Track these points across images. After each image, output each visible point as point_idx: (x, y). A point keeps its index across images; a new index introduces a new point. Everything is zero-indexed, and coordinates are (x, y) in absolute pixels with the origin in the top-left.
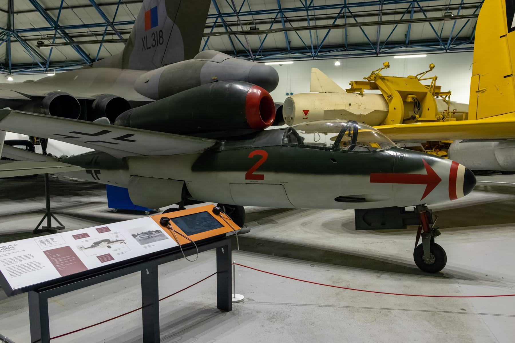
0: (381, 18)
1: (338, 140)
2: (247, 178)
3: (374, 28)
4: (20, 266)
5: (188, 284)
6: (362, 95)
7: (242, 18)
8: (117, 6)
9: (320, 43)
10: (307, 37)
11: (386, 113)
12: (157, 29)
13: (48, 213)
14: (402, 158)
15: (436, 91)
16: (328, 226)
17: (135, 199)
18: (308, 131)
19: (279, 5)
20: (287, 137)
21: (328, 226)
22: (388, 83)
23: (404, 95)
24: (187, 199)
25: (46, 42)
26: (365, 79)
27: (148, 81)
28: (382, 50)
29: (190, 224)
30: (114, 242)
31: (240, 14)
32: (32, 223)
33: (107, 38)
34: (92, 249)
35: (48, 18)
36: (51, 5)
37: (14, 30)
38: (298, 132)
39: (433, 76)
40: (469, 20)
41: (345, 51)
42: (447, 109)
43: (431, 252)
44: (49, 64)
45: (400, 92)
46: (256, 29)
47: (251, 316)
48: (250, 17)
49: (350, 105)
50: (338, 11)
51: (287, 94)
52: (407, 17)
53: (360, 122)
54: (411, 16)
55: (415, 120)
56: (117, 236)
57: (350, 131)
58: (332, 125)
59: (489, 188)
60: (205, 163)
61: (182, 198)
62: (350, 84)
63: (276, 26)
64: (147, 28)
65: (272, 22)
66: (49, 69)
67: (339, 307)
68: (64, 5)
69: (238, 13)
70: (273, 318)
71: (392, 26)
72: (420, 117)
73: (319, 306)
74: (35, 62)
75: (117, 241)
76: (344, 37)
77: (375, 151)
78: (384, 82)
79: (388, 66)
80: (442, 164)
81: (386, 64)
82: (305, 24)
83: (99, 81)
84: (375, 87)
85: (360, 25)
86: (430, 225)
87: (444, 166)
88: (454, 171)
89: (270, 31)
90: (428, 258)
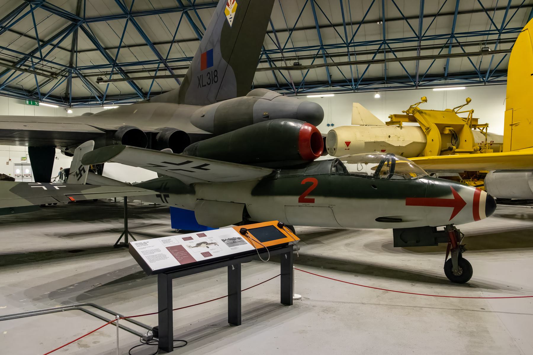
0: (420, 53)
1: (378, 170)
2: (300, 201)
3: (413, 63)
4: (153, 256)
5: (261, 283)
6: (401, 127)
7: (286, 55)
8: (170, 44)
9: (360, 76)
10: (347, 72)
11: (425, 144)
12: (212, 68)
13: (126, 232)
14: (433, 185)
15: (473, 123)
16: (369, 246)
17: (200, 220)
18: (352, 161)
19: (321, 41)
20: (334, 167)
21: (369, 246)
22: (426, 117)
23: (441, 127)
24: (247, 218)
25: (105, 78)
26: (403, 112)
27: (204, 116)
28: (421, 83)
29: (261, 234)
30: (210, 244)
31: (284, 51)
32: (111, 239)
33: (159, 73)
34: (196, 248)
35: (108, 57)
36: (110, 45)
37: (76, 67)
38: (343, 162)
39: (470, 109)
40: (506, 55)
41: (384, 83)
42: (484, 140)
43: (459, 265)
44: (106, 98)
45: (438, 125)
46: (299, 65)
47: (308, 309)
48: (293, 54)
49: (389, 136)
50: (377, 47)
51: (328, 125)
52: (445, 51)
53: (398, 154)
54: (450, 51)
55: (452, 151)
56: (212, 240)
57: (388, 162)
58: (373, 157)
59: (526, 216)
60: (263, 188)
61: (243, 218)
62: (389, 117)
63: (318, 61)
64: (202, 69)
65: (314, 57)
66: (105, 102)
67: (379, 305)
68: (123, 44)
69: (283, 49)
70: (326, 310)
71: (430, 61)
72: (457, 148)
73: (363, 304)
74: (93, 95)
75: (212, 243)
76: (384, 71)
77: (410, 179)
78: (422, 116)
79: (426, 101)
80: (468, 190)
81: (424, 99)
82: (345, 59)
83: (158, 115)
84: (413, 119)
85: (400, 60)
86: (458, 243)
87: (469, 192)
88: (477, 196)
89: (312, 66)
90: (457, 271)
